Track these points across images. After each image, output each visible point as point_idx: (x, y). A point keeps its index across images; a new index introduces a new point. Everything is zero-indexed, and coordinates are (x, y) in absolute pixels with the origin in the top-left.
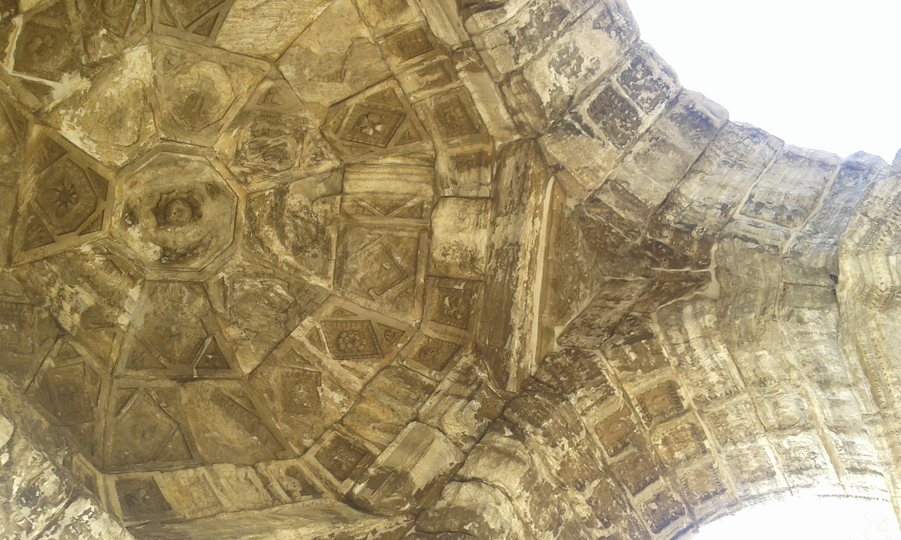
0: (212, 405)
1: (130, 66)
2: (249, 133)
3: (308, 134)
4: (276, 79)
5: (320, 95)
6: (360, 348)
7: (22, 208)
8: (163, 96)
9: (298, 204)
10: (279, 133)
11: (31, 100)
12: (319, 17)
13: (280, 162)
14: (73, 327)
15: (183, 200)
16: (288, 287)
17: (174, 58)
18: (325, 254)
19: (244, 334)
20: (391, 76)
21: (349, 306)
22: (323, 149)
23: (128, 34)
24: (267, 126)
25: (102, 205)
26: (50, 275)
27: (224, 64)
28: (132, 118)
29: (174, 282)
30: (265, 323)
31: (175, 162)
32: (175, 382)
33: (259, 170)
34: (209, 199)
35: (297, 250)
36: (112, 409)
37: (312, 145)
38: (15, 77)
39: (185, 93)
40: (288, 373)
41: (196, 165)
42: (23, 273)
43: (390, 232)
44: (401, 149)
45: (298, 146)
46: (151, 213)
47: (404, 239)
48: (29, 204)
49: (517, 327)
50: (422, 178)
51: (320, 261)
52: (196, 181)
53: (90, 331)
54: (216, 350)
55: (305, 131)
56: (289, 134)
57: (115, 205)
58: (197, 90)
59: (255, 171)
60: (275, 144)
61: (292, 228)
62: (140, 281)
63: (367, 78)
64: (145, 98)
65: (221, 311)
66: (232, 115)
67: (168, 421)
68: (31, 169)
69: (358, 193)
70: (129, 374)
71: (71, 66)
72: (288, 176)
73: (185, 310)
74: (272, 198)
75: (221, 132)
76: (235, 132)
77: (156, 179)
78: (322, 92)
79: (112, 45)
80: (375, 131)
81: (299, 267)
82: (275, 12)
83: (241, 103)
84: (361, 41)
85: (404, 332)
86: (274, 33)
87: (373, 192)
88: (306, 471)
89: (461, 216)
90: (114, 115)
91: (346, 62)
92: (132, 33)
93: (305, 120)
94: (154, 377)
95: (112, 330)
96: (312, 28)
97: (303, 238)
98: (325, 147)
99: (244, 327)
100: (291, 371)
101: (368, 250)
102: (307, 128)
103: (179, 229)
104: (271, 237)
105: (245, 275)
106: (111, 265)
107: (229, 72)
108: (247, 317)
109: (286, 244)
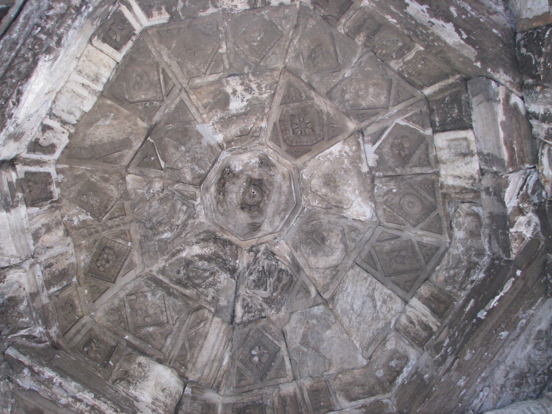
0: (125, 136)
1: (362, 204)
2: (283, 268)
3: (268, 307)
4: (314, 300)
5: (295, 326)
6: (99, 262)
7: (313, 94)
8: (333, 219)
9: (219, 280)
10: (275, 290)
11: (373, 129)
12: (353, 341)
13: (254, 281)
14: (228, 82)
15: (259, 203)
16: (165, 242)
17: (355, 235)
18: (177, 280)
19: (152, 192)
20: (295, 379)
21: (132, 275)
22: (253, 314)
23: (385, 207)
24: (284, 282)
25: (284, 147)
26: (264, 89)
27: (340, 266)
28: (327, 194)
29: (211, 167)
30: (151, 210)
31: (285, 210)
32: (154, 123)
33: (255, 263)
34: (250, 221)
35: (188, 263)
36: (168, 71)
37: (259, 307)
38: (392, 123)
39: (328, 235)
40: (111, 201)
41: (276, 224)
42: (276, 74)
43: (173, 333)
44: (234, 371)
45: (261, 297)
46: (261, 178)
47: (163, 341)
48: (313, 99)
49: (63, 383)
50: (205, 376)
51: (173, 274)
52: (266, 218)
53: (218, 92)
54: (156, 165)
55: (271, 306)
56: (272, 295)
57: (279, 156)
58: (327, 243)
59: (256, 260)
60: (268, 283)
61: (204, 267)
62: (225, 145)
63: (298, 362)
64: (337, 207)
65: (176, 186)
66: (301, 261)
67: (136, 99)
68: (332, 112)
69: (210, 326)
70: (178, 99)
71: (380, 162)
72: (243, 281)
73: (190, 164)
74: (232, 264)
75: (292, 249)
76: (288, 258)
77: (280, 193)
78: (296, 327)
79: (382, 194)
80: (254, 356)
81: (176, 258)
82: (365, 311)
83: (307, 271)
84: (327, 365)
85: (94, 302)
86: (349, 307)
87: (206, 337)
88: (46, 157)
89: (167, 391)
90: (335, 182)
91: (314, 351)
92: (384, 209)
93: (278, 310)
94: (165, 112)
95: (208, 107)
96: (345, 335)
97: (194, 271)
98: (254, 316)
99: (156, 195)
100: (112, 204)
101: (166, 311)
102: (273, 308)
103: (242, 190)
104: (205, 249)
105: (189, 217)
106: (245, 133)
107: (332, 269)
108: (162, 201)
109: (196, 258)
